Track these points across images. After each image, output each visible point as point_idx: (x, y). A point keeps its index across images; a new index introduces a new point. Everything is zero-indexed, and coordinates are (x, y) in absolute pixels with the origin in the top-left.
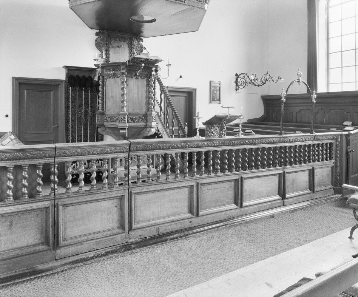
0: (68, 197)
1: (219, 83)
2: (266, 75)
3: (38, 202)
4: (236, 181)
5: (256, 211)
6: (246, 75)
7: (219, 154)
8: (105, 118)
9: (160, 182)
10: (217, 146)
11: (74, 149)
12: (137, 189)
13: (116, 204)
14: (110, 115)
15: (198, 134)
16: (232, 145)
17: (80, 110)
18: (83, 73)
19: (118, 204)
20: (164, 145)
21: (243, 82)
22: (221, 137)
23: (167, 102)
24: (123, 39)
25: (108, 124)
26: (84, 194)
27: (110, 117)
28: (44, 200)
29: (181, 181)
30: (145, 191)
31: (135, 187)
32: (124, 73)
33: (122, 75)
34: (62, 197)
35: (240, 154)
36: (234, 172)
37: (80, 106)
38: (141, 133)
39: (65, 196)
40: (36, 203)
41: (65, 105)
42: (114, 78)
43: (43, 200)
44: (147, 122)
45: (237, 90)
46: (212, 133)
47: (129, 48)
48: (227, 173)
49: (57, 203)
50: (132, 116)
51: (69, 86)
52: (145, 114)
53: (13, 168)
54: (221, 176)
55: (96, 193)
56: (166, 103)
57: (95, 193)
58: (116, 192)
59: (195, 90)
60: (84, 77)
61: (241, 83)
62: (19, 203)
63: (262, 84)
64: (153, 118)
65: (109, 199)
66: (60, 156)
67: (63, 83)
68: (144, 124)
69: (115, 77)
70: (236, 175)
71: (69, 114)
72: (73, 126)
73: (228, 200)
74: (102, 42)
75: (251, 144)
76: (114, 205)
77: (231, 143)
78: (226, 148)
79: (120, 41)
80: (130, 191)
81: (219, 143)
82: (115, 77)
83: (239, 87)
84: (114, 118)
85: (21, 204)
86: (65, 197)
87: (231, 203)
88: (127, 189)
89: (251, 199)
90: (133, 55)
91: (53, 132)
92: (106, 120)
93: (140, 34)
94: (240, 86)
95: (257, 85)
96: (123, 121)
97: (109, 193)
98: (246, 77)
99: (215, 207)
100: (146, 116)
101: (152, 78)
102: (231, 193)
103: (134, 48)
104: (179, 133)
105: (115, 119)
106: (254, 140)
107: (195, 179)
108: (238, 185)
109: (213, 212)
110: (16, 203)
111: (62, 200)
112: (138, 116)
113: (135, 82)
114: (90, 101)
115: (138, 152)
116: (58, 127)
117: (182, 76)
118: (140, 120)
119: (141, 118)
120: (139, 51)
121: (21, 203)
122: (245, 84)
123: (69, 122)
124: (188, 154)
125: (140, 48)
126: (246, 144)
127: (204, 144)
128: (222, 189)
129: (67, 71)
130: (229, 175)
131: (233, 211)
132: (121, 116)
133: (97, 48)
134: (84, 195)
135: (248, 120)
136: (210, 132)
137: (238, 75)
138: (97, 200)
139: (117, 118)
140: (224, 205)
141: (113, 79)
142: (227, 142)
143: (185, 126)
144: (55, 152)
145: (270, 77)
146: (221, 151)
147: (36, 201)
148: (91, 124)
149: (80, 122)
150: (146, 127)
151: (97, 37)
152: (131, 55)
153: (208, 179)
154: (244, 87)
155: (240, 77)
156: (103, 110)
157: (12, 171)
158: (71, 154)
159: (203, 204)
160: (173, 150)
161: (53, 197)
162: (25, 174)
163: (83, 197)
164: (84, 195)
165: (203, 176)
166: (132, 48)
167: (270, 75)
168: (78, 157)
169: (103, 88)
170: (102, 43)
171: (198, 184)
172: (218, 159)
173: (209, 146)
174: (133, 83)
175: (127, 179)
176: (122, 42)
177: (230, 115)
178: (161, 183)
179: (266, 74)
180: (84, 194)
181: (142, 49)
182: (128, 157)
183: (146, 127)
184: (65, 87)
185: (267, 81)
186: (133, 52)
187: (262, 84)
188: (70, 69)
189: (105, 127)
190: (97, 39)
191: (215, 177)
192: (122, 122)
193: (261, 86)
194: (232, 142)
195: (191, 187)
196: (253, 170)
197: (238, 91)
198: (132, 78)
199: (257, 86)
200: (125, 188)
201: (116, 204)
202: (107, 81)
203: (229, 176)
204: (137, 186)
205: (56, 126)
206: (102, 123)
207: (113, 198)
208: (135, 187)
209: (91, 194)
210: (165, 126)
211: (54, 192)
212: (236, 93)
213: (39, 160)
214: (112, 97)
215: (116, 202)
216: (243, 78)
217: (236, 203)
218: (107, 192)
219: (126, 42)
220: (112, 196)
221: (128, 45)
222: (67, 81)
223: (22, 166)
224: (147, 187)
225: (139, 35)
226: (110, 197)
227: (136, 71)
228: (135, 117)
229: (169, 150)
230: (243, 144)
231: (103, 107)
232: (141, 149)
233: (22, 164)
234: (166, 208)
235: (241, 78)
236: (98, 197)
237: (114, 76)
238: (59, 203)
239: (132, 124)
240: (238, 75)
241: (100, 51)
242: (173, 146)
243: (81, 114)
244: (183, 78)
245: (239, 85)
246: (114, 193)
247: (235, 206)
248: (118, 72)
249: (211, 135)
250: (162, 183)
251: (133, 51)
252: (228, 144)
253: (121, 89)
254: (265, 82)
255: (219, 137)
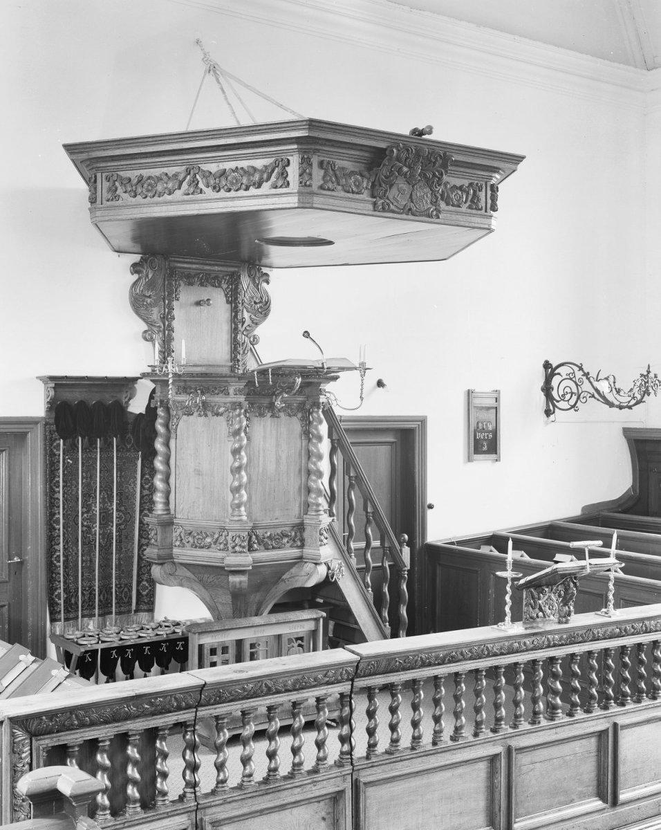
0: (225, 802)
1: (495, 395)
2: (645, 376)
3: (164, 818)
4: (601, 735)
5: (651, 812)
6: (581, 369)
7: (558, 666)
8: (174, 534)
9: (422, 750)
10: (555, 645)
11: (239, 684)
12: (369, 771)
13: (323, 814)
14: (191, 529)
15: (508, 618)
16: (591, 641)
17: (88, 507)
18: (96, 392)
19: (329, 813)
20: (433, 654)
21: (568, 390)
22: (567, 622)
23: (352, 475)
24: (209, 280)
25: (185, 554)
26: (257, 794)
27: (190, 534)
28: (176, 813)
29: (470, 746)
30: (388, 776)
31: (365, 768)
32: (240, 405)
33: (235, 409)
34: (213, 804)
35: (610, 661)
36: (597, 712)
37: (88, 495)
38: (284, 577)
39: (218, 799)
40: (159, 822)
41: (46, 495)
42: (206, 415)
43: (173, 813)
44: (302, 546)
45: (548, 413)
46: (541, 609)
47: (229, 306)
48: (580, 714)
49: (201, 819)
50: (261, 531)
51: (56, 435)
52: (297, 521)
53: (110, 740)
54: (564, 726)
55: (282, 788)
56: (347, 477)
57: (279, 788)
58: (325, 782)
59: (423, 421)
60: (100, 404)
61: (561, 393)
62: (126, 825)
63: (631, 404)
64: (321, 534)
65: (308, 801)
66: (208, 704)
67: (39, 428)
68: (295, 552)
69: (209, 413)
70: (601, 721)
71: (58, 522)
72: (68, 559)
73: (580, 789)
74: (150, 293)
75: (638, 633)
76: (318, 816)
77: (590, 634)
78: (576, 648)
79: (202, 285)
80: (354, 778)
81: (561, 639)
82: (209, 413)
83: (554, 406)
84: (207, 536)
85: (129, 826)
86: (217, 802)
87: (590, 796)
88: (349, 774)
89: (637, 783)
90: (240, 326)
91: (7, 579)
92: (178, 543)
93: (260, 260)
94: (558, 401)
95: (617, 403)
96: (237, 549)
97: (310, 786)
98: (579, 374)
99: (549, 807)
100: (300, 527)
101: (317, 412)
102: (588, 769)
103: (243, 304)
104: (367, 561)
105: (208, 540)
106: (647, 623)
107: (503, 737)
108: (608, 743)
109: (546, 823)
110: (120, 824)
111: (209, 811)
112: (279, 531)
113: (269, 429)
114: (117, 477)
115: (373, 677)
116: (21, 563)
117: (385, 382)
118: (285, 540)
119: (287, 536)
120: (256, 312)
121: (130, 824)
122: (575, 398)
123: (56, 547)
124: (484, 673)
125: (261, 302)
126: (627, 634)
127: (525, 644)
128: (568, 758)
129: (52, 393)
130: (584, 721)
131: (596, 816)
132: (234, 534)
133: (137, 313)
134: (255, 796)
135: (584, 509)
136: (533, 608)
137: (554, 366)
138: (282, 807)
139: (216, 536)
140: (572, 801)
141: (203, 417)
142: (580, 632)
143: (401, 544)
144: (201, 695)
145: (657, 382)
146: (563, 659)
147: (161, 816)
148: (119, 550)
149: (88, 544)
150: (300, 559)
151: (136, 277)
152: (233, 325)
153: (534, 734)
154: (573, 407)
155: (559, 374)
156: (168, 510)
157: (107, 748)
158: (231, 698)
159: (522, 802)
160: (451, 665)
161: (193, 804)
162: (132, 752)
163: (256, 801)
164: (255, 796)
165: (521, 728)
166: (236, 307)
167: (656, 376)
168: (243, 701)
169: (167, 445)
170: (149, 297)
171: (509, 750)
172: (556, 680)
173: (535, 649)
174: (265, 432)
175: (346, 749)
176: (210, 289)
177: (590, 564)
178: (424, 753)
179: (645, 373)
180: (257, 794)
181: (266, 307)
182: (349, 693)
183: (300, 559)
184: (45, 439)
185: (649, 394)
186: (239, 317)
187: (633, 402)
188: (59, 384)
189: (174, 563)
190: (135, 284)
191: (550, 729)
192: (236, 552)
193: (630, 408)
194: (593, 633)
195: (493, 759)
196: (643, 704)
197: (552, 417)
198: (262, 415)
199: (617, 407)
200: (343, 773)
201: (323, 814)
202: (181, 423)
203: (585, 724)
204: (370, 765)
205: (16, 559)
206: (167, 551)
207: (318, 799)
208: (365, 768)
209: (273, 792)
210: (345, 549)
211: (195, 793)
212: (547, 424)
213: (165, 717)
214: (198, 473)
215: (322, 809)
216: (571, 379)
217: (601, 795)
218: (306, 784)
219: (220, 286)
220: (317, 794)
221: (226, 296)
222: (52, 421)
223: (130, 733)
224: (392, 765)
225: (257, 263)
226: (312, 796)
227: (274, 394)
228: (269, 534)
229: (442, 666)
230: (619, 636)
231: (167, 503)
232: (381, 670)
233: (131, 730)
234: (435, 816)
235: (561, 379)
236: (287, 797)
237: (205, 408)
238: (207, 819)
239: (262, 554)
240: (554, 366)
241: (144, 320)
242: (452, 657)
243: (92, 519)
244: (379, 378)
245: (558, 399)
246: (319, 786)
247: (599, 804)
248: (219, 399)
249: (538, 617)
250: (427, 754)
251: (240, 314)
252: (583, 637)
253: (230, 454)
254: (642, 398)
255: (560, 622)
